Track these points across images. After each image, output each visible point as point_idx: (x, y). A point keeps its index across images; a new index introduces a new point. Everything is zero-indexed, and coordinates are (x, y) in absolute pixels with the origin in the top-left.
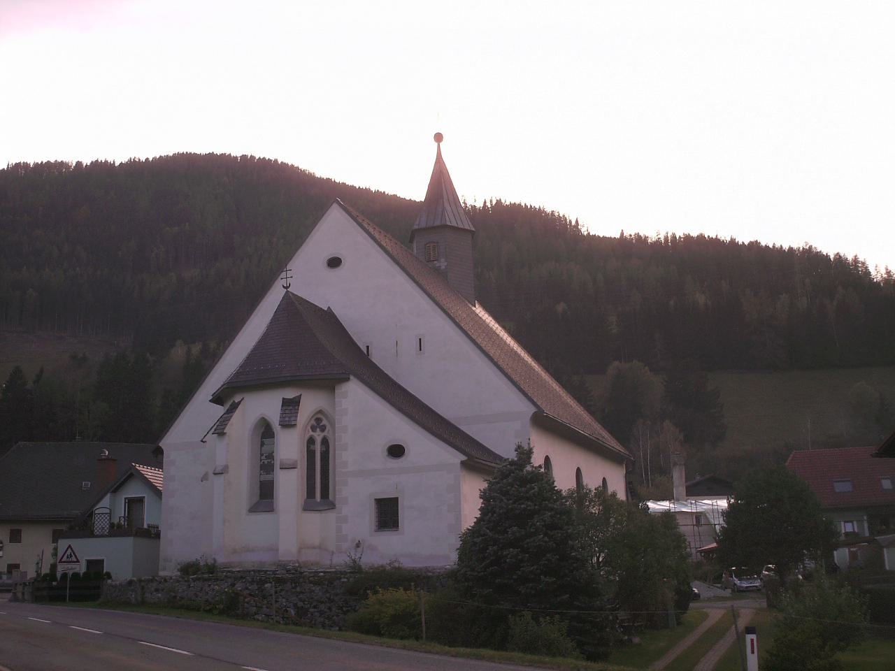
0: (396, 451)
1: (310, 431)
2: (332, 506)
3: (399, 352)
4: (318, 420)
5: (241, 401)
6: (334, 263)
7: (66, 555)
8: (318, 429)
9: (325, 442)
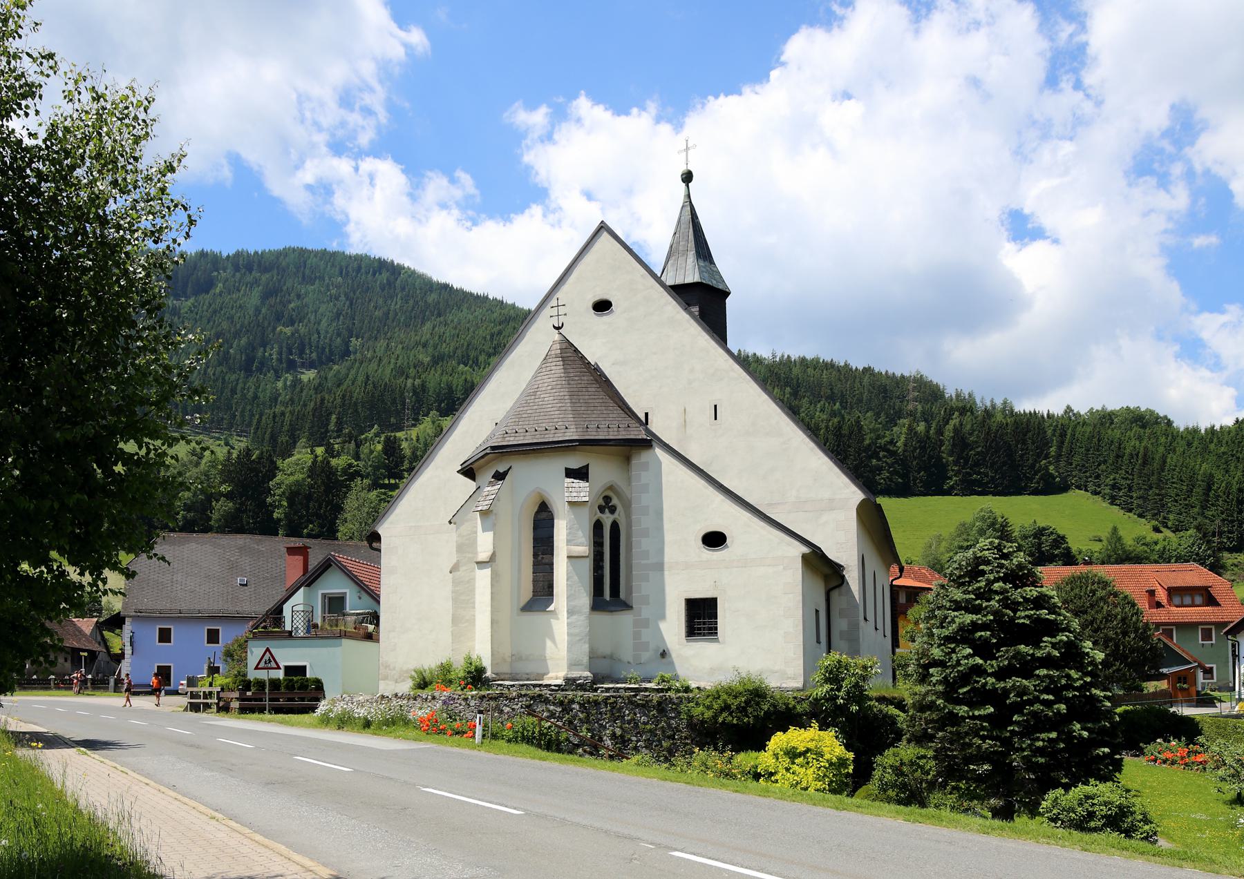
0: (714, 540)
1: (598, 511)
2: (627, 606)
3: (687, 420)
4: (607, 499)
5: (509, 470)
6: (602, 306)
7: (264, 660)
8: (607, 510)
9: (615, 527)
